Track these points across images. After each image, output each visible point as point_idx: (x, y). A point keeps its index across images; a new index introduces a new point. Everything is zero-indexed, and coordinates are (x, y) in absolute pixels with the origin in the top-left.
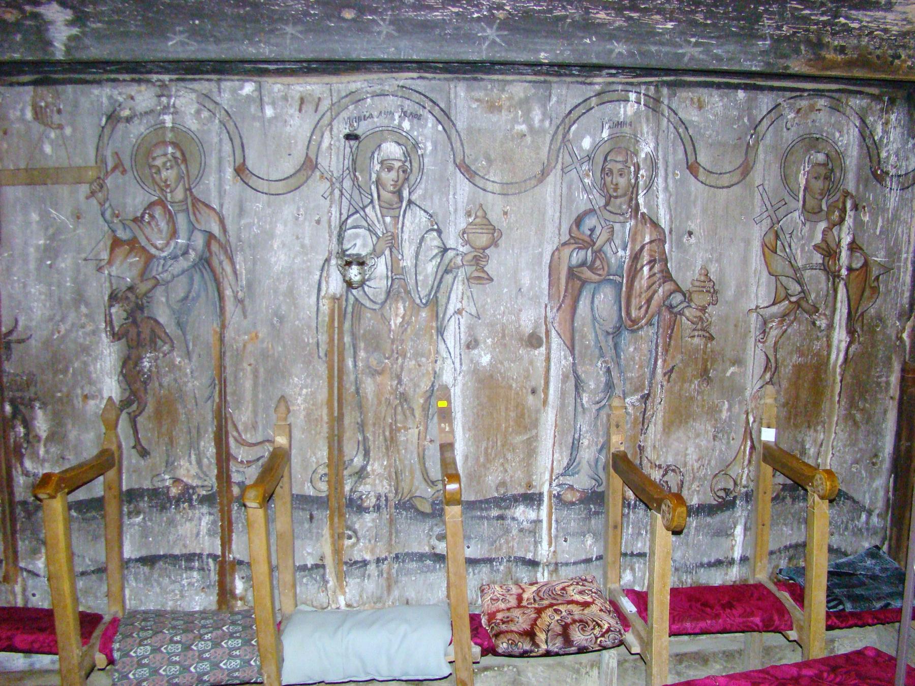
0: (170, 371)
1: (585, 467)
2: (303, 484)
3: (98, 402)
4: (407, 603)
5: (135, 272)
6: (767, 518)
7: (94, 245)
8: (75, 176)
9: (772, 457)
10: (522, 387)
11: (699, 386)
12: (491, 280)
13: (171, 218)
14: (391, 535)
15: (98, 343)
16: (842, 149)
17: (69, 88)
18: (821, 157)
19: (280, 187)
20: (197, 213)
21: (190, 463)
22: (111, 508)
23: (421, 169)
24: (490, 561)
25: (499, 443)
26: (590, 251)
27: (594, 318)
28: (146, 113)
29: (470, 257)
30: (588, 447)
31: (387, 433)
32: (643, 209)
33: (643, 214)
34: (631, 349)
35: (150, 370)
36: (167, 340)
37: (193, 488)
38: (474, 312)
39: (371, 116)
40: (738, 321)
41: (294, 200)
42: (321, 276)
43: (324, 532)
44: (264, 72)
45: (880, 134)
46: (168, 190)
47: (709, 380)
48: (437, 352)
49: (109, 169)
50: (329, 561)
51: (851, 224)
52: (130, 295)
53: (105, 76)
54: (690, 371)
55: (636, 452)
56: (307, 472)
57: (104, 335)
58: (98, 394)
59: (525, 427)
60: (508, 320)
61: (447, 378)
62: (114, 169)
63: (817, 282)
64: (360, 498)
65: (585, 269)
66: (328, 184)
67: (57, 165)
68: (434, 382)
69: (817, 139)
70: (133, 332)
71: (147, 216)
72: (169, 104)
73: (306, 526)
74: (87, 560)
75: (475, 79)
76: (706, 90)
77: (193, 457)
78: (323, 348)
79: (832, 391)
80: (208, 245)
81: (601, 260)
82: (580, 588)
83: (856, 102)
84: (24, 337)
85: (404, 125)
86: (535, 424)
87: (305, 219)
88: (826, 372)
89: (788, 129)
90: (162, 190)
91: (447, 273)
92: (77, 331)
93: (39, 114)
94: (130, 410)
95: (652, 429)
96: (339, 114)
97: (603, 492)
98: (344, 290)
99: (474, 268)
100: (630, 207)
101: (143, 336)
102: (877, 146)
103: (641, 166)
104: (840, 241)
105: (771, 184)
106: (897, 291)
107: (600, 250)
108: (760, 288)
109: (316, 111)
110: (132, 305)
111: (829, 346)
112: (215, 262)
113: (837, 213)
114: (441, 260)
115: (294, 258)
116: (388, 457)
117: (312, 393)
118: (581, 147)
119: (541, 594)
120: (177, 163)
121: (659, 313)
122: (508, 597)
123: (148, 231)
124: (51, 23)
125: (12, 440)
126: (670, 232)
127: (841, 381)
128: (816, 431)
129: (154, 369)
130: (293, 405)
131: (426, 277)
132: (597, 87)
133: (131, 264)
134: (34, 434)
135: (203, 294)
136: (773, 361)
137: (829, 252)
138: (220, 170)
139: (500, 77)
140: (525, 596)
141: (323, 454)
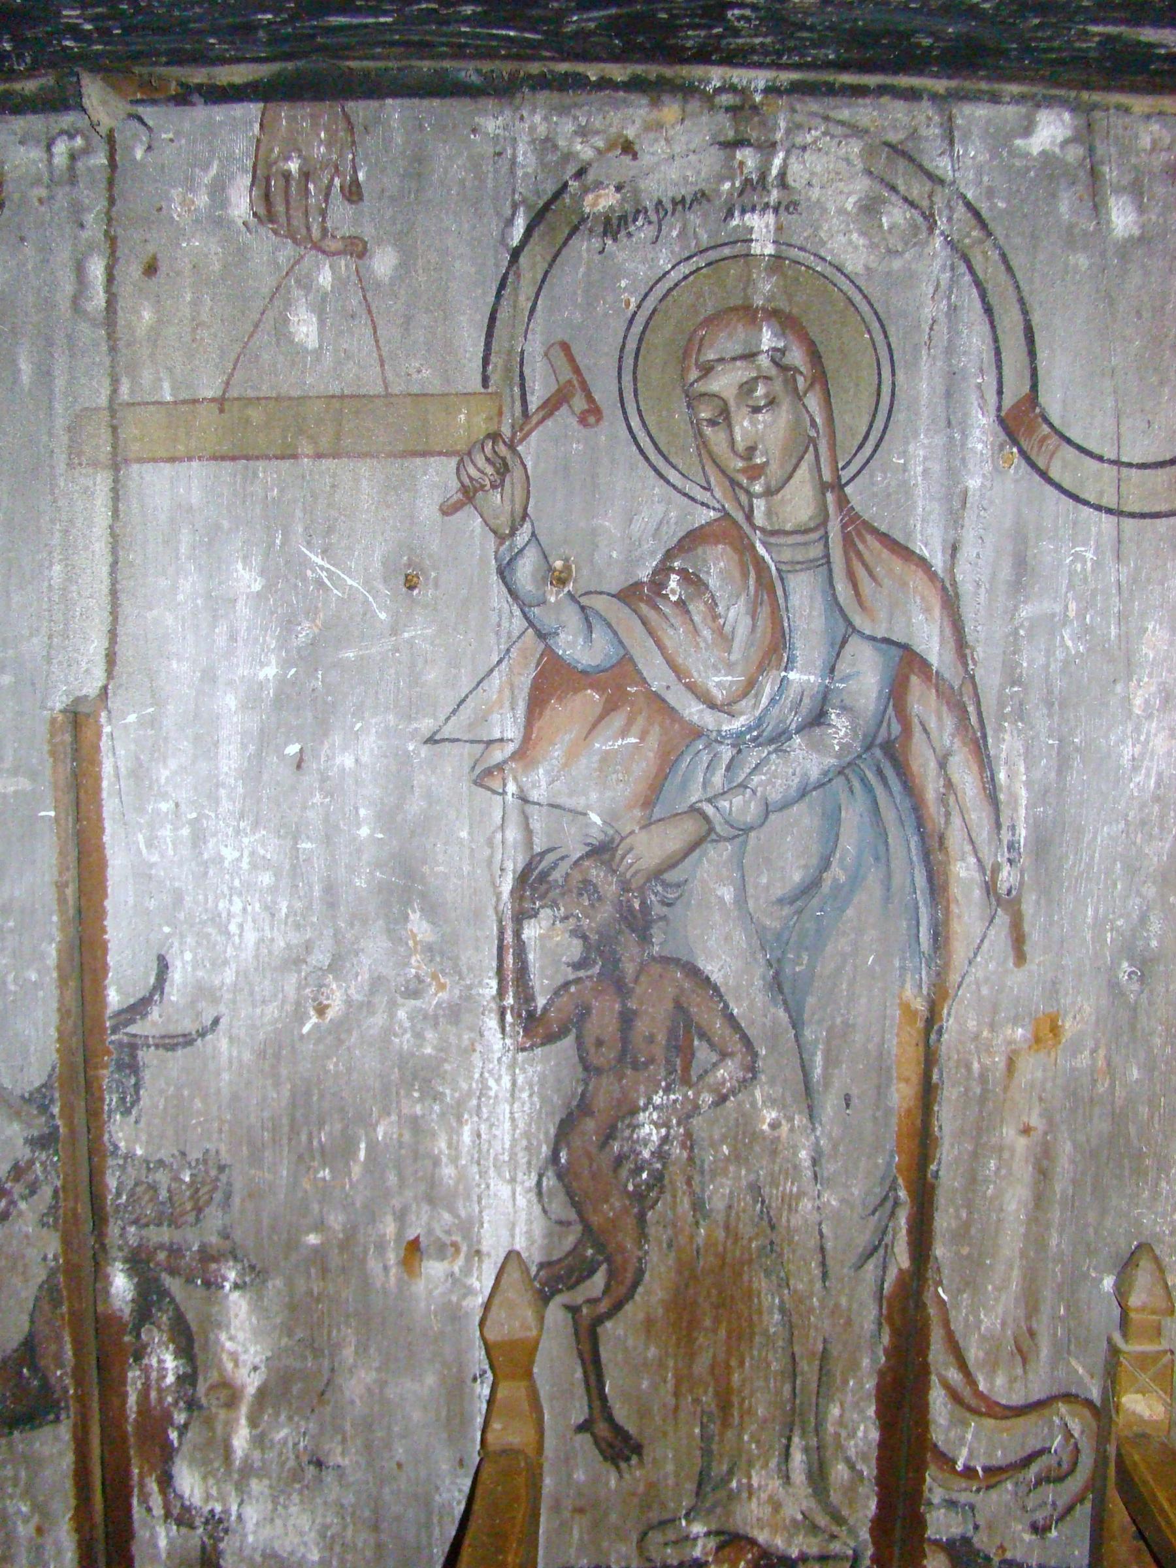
0: (737, 1157)
3: (457, 1266)
5: (624, 788)
7: (465, 686)
13: (767, 589)
17: (395, 110)
20: (861, 573)
28: (680, 203)
35: (660, 1154)
46: (758, 488)
49: (534, 403)
52: (596, 873)
57: (492, 1023)
58: (463, 1243)
62: (551, 406)
67: (335, 388)
71: (674, 581)
77: (798, 1457)
80: (896, 693)
84: (188, 1025)
90: (734, 483)
92: (392, 1005)
93: (274, 200)
94: (578, 1296)
101: (642, 1026)
110: (606, 912)
112: (923, 762)
123: (675, 636)
125: (132, 1399)
129: (676, 1151)
133: (606, 758)
134: (214, 1376)
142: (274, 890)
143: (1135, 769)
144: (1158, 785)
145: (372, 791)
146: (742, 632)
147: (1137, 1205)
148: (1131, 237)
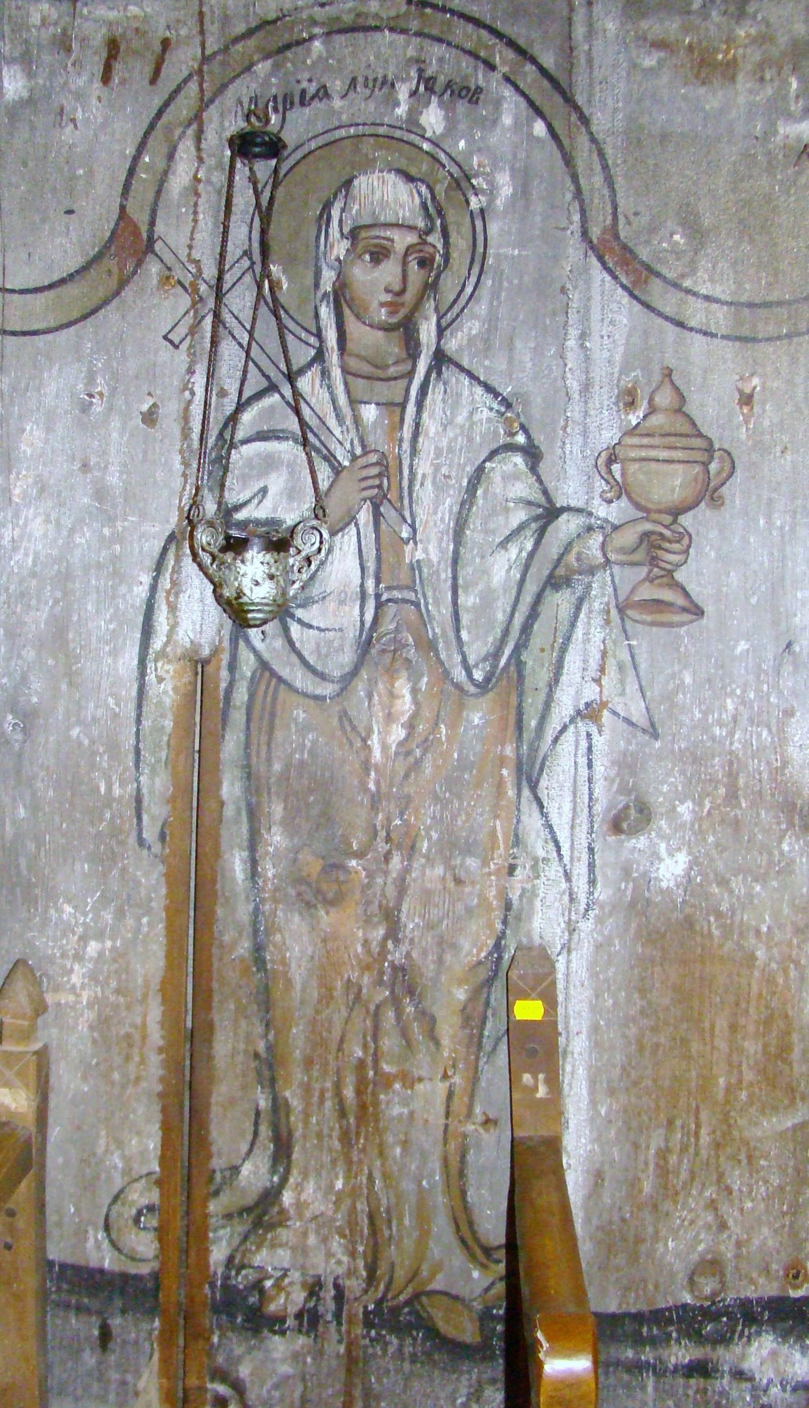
2: (81, 1235)
12: (699, 612)
23: (478, 258)
25: (705, 1138)
29: (628, 537)
31: (349, 1093)
38: (637, 711)
39: (323, 93)
42: (153, 588)
43: (141, 1384)
48: (517, 841)
59: (791, 1091)
60: (747, 744)
61: (545, 924)
64: (257, 1286)
68: (502, 936)
73: (90, 1359)
85: (424, 120)
87: (110, 409)
91: (557, 587)
96: (223, 87)
98: (226, 633)
99: (644, 571)
109: (153, 81)
114: (537, 543)
115: (72, 531)
116: (349, 1162)
117: (118, 955)
130: (57, 989)
131: (488, 599)
141: (146, 1144)
143: (15, 549)
144: (35, 563)
147: (31, 930)
148: (21, 99)
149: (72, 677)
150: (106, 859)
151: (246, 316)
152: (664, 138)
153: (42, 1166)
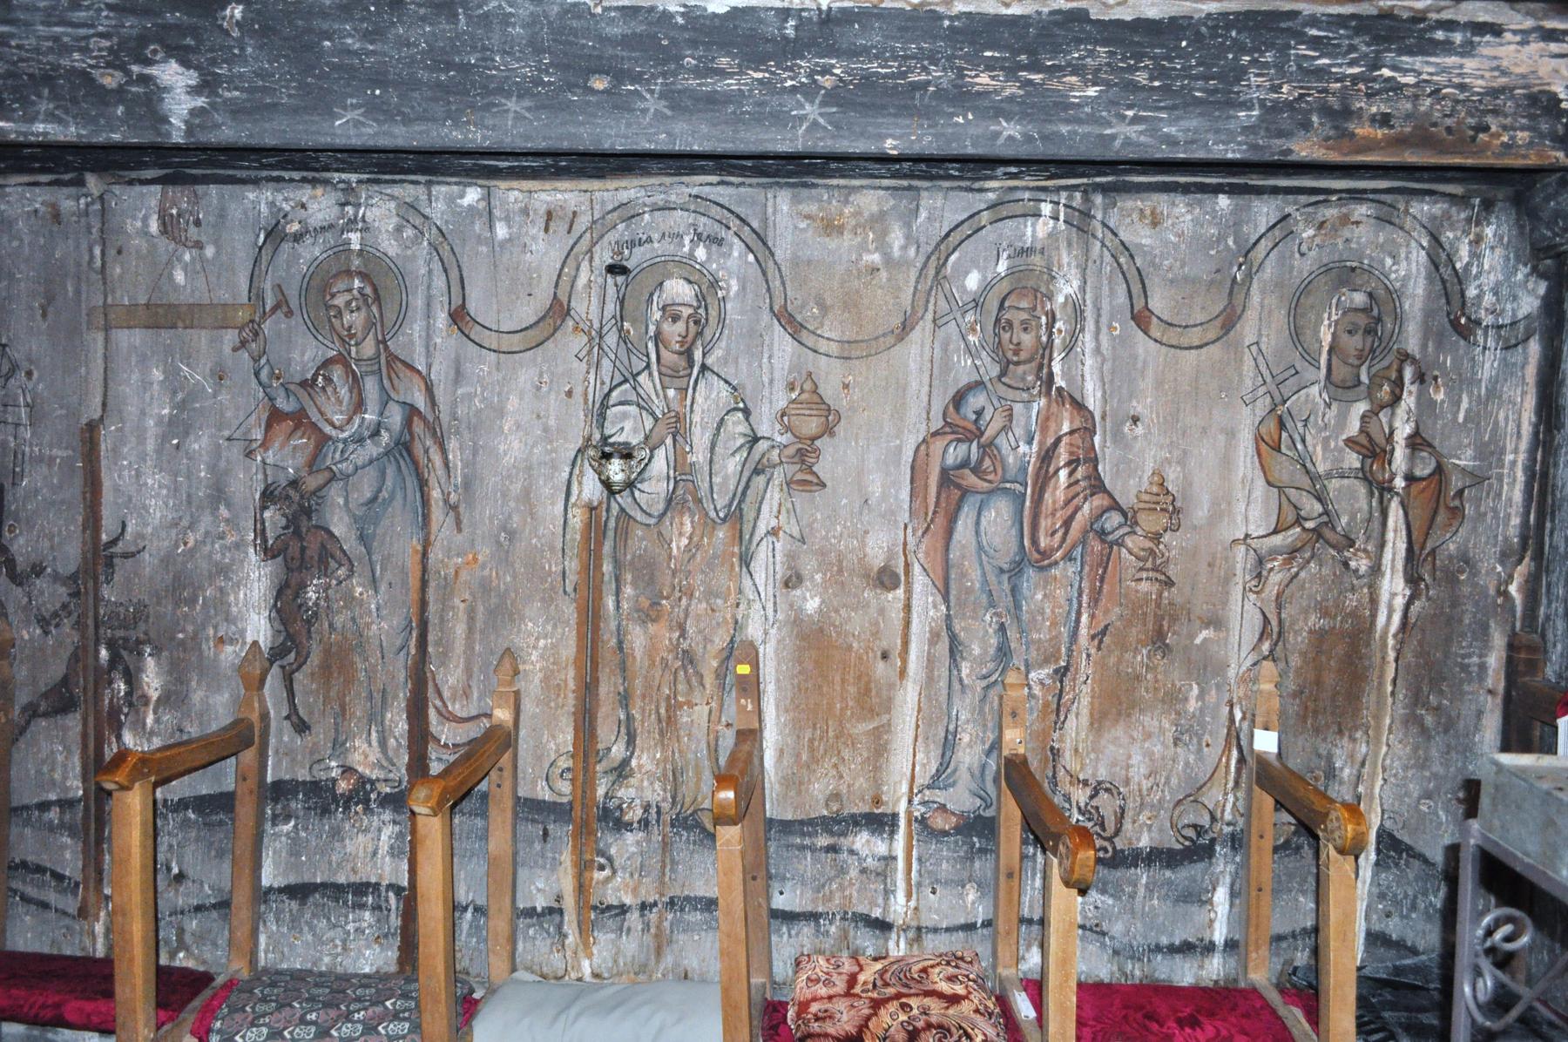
1: (964, 777)
2: (534, 783)
4: (686, 977)
5: (301, 459)
6: (1266, 878)
8: (218, 316)
9: (1266, 775)
10: (868, 649)
11: (1149, 657)
12: (824, 485)
13: (356, 383)
14: (663, 867)
15: (242, 562)
16: (1398, 285)
17: (213, 189)
18: (1359, 298)
19: (515, 342)
21: (370, 745)
22: (245, 810)
23: (721, 320)
24: (813, 917)
25: (831, 734)
26: (975, 444)
27: (980, 547)
28: (323, 228)
29: (791, 451)
30: (970, 745)
31: (662, 711)
32: (1060, 382)
33: (1060, 389)
34: (1039, 596)
35: (316, 604)
36: (344, 561)
37: (372, 782)
38: (796, 533)
39: (650, 240)
40: (1214, 558)
41: (535, 360)
44: (495, 173)
45: (1466, 259)
47: (1166, 649)
48: (740, 592)
49: (268, 308)
50: (569, 903)
51: (1413, 406)
52: (292, 493)
53: (264, 173)
54: (1134, 633)
55: (1047, 758)
56: (544, 758)
59: (872, 710)
60: (847, 547)
61: (754, 631)
62: (275, 309)
63: (1352, 501)
64: (620, 807)
65: (967, 471)
66: (586, 339)
67: (191, 301)
69: (1353, 269)
70: (294, 549)
72: (356, 216)
73: (538, 846)
74: (206, 887)
75: (805, 185)
76: (1164, 197)
77: (374, 735)
78: (572, 579)
79: (1381, 676)
80: (408, 423)
81: (993, 458)
82: (951, 970)
83: (1423, 209)
84: (133, 549)
86: (888, 706)
88: (1368, 645)
89: (1302, 255)
92: (213, 543)
93: (168, 226)
94: (285, 662)
95: (1071, 723)
96: (602, 236)
97: (993, 819)
100: (1039, 378)
102: (1460, 279)
103: (1058, 316)
104: (1392, 433)
105: (1273, 343)
106: (1496, 517)
107: (991, 444)
108: (1252, 506)
110: (295, 507)
111: (1374, 601)
112: (418, 450)
113: (1386, 388)
117: (554, 646)
118: (964, 286)
119: (887, 976)
120: (366, 301)
121: (1084, 543)
122: (835, 978)
124: (167, 89)
126: (1103, 418)
127: (1397, 660)
128: (1353, 740)
129: (322, 603)
131: (726, 478)
132: (991, 196)
133: (295, 447)
135: (399, 496)
136: (1274, 623)
137: (1373, 450)
138: (428, 315)
139: (842, 182)
140: (862, 978)
141: (566, 738)
142: (167, 496)
145: (205, 458)
146: (346, 399)
149: (532, 515)
150: (548, 601)
151: (613, 346)
152: (809, 262)
153: (516, 748)
